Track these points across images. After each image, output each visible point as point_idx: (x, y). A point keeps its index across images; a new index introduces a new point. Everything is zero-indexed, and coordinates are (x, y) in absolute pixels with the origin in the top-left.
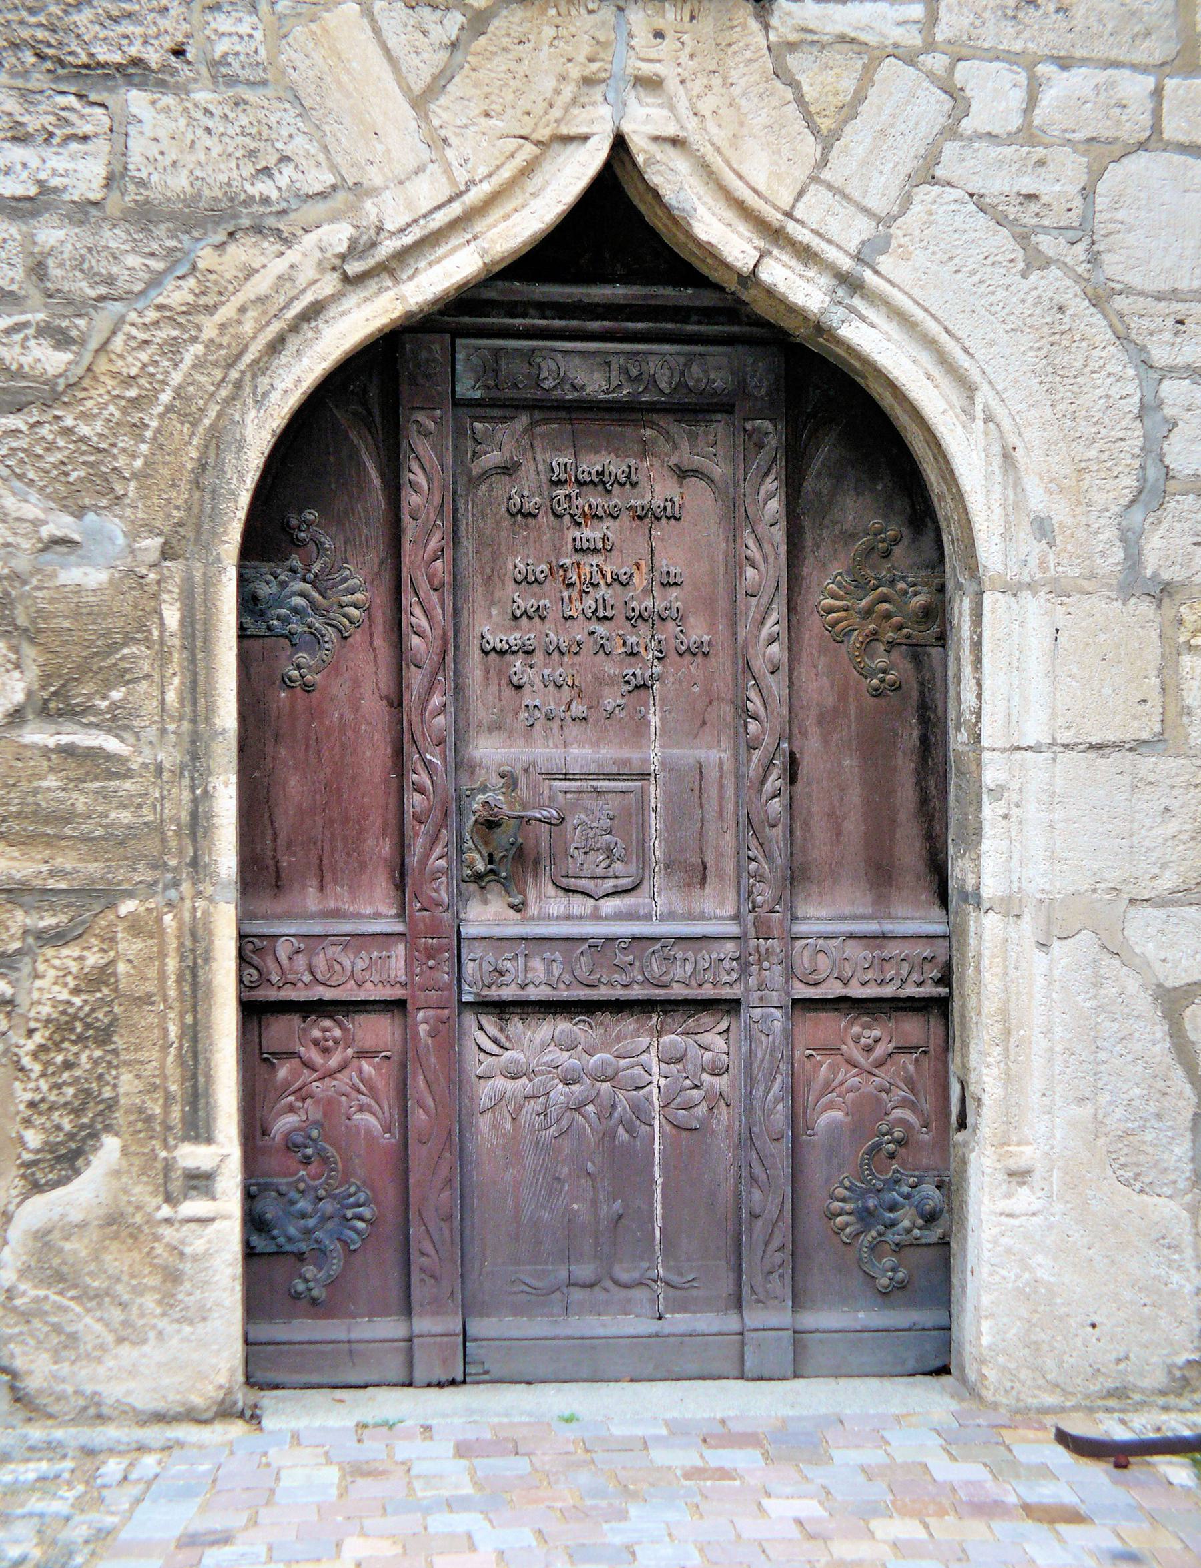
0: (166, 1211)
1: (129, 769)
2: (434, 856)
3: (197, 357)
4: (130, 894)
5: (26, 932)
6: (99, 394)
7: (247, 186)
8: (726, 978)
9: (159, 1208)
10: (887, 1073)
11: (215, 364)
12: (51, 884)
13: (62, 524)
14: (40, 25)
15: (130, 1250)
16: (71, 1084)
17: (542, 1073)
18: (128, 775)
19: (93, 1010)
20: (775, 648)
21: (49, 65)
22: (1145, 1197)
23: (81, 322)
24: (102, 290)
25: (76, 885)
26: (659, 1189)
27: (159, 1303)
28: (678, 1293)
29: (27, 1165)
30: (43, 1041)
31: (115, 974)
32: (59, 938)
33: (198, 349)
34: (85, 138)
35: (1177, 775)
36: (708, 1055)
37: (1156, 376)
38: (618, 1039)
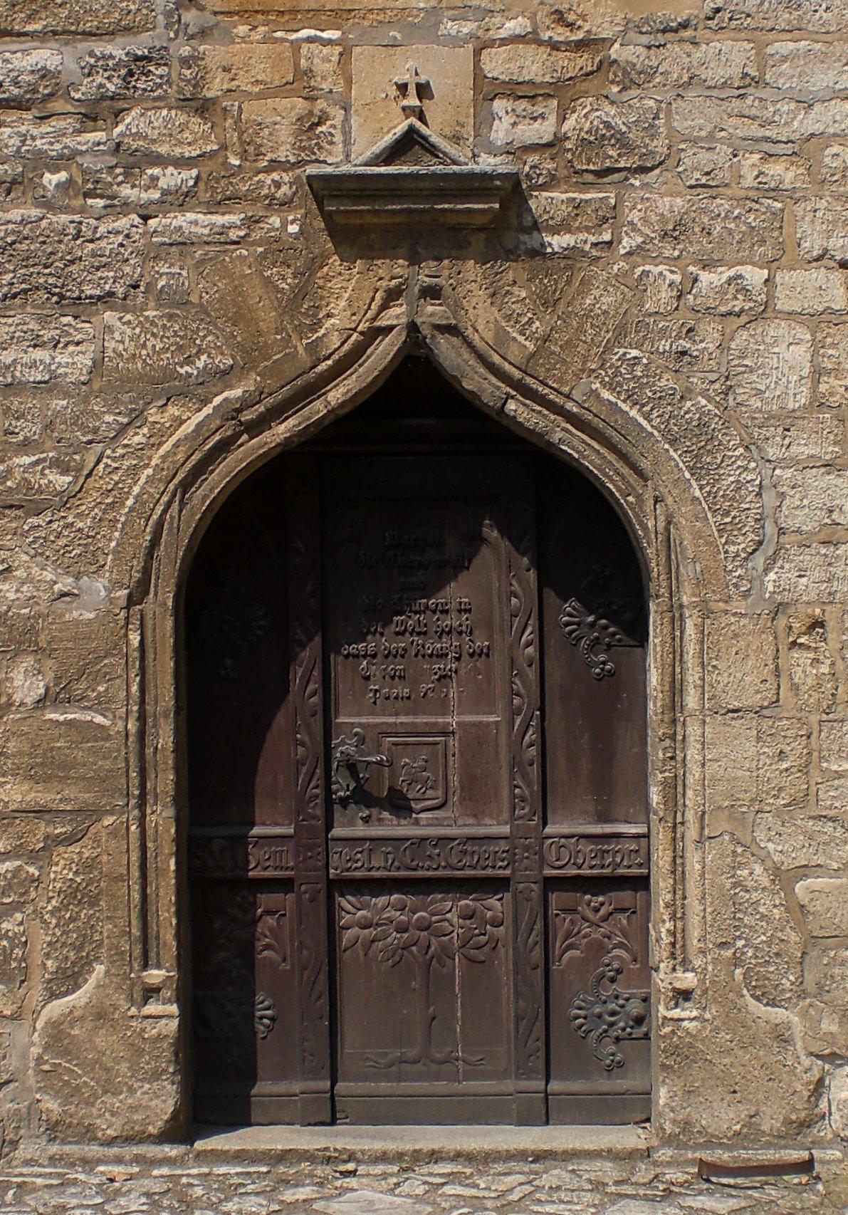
0: (133, 1011)
1: (109, 735)
2: (311, 786)
3: (148, 476)
4: (112, 813)
5: (47, 837)
6: (89, 502)
7: (178, 369)
8: (501, 864)
9: (129, 1009)
10: (609, 925)
11: (160, 480)
12: (62, 807)
13: (65, 584)
14: (50, 274)
15: (111, 1036)
16: (74, 932)
17: (382, 925)
18: (108, 738)
19: (87, 886)
20: (530, 650)
21: (55, 299)
22: (769, 1008)
23: (77, 457)
24: (90, 437)
25: (76, 807)
26: (459, 1001)
27: (129, 1069)
28: (471, 1068)
29: (50, 981)
30: (57, 905)
31: (100, 863)
32: (70, 840)
33: (149, 471)
34: (78, 344)
35: (788, 729)
36: (489, 914)
37: (772, 466)
38: (432, 903)
